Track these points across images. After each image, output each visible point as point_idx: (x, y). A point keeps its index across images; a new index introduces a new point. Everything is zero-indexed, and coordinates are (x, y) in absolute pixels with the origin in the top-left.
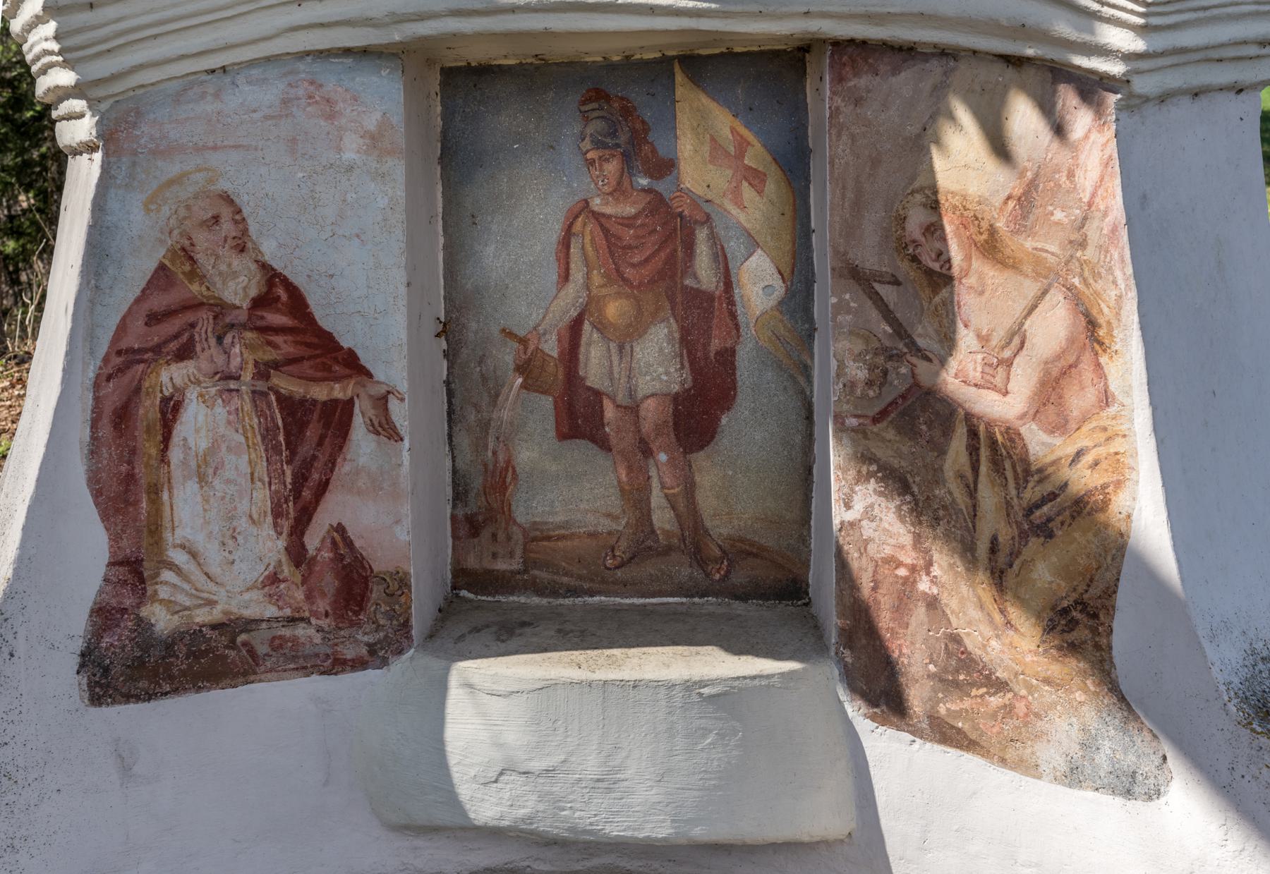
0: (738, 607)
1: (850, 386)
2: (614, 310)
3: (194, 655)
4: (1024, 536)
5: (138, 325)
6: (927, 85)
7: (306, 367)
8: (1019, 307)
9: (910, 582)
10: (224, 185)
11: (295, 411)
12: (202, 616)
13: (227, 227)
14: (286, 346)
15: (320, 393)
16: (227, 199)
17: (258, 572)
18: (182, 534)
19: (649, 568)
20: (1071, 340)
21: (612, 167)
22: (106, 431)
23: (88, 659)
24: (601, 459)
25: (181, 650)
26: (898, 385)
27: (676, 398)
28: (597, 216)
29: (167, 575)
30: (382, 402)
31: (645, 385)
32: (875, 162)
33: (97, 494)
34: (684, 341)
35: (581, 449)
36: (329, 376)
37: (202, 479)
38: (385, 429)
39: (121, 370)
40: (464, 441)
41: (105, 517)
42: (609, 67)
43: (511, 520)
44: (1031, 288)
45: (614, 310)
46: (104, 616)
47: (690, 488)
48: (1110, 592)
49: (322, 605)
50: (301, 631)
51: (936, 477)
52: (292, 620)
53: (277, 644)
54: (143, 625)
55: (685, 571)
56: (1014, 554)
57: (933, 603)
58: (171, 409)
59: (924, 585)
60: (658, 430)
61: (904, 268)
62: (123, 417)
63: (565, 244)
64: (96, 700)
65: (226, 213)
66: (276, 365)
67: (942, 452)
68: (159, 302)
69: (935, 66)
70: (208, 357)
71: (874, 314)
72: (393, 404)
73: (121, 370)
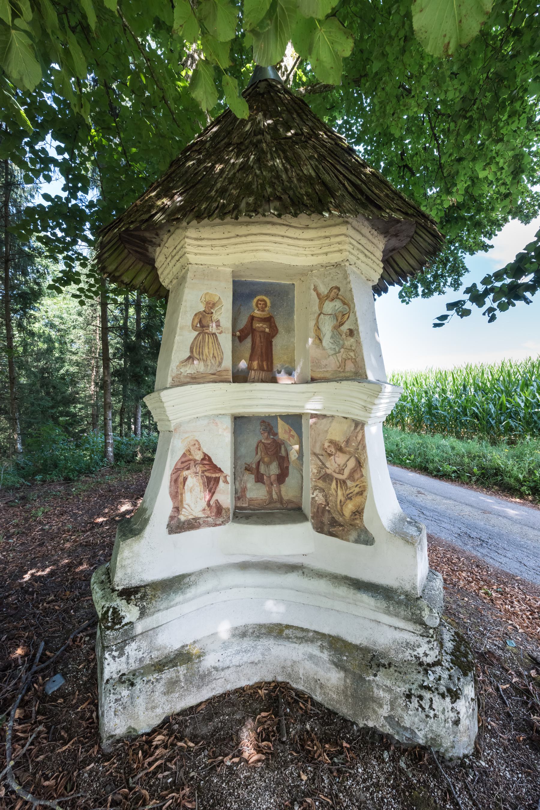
0: (289, 512)
1: (314, 474)
2: (266, 459)
3: (189, 524)
4: (346, 499)
5: (179, 464)
6: (329, 421)
7: (211, 471)
8: (346, 459)
9: (325, 508)
10: (196, 438)
11: (209, 479)
12: (191, 517)
13: (197, 446)
14: (207, 467)
15: (214, 475)
16: (197, 441)
17: (201, 508)
18: (187, 502)
19: (272, 506)
20: (356, 466)
21: (266, 434)
22: (173, 483)
23: (168, 526)
24: (263, 486)
25: (186, 523)
26: (323, 473)
27: (278, 475)
28: (263, 443)
29: (184, 510)
30: (225, 477)
31: (272, 473)
32: (319, 435)
33: (171, 495)
34: (279, 465)
35: (259, 485)
36: (215, 472)
37: (191, 492)
38: (226, 482)
39: (176, 472)
40: (237, 483)
41: (172, 499)
42: (266, 417)
43: (246, 497)
44: (348, 456)
45: (266, 459)
46: (172, 518)
47: (280, 491)
48: (363, 509)
49: (213, 514)
50: (209, 519)
51: (330, 489)
52: (207, 517)
53: (204, 522)
54: (179, 519)
55: (279, 505)
56: (344, 503)
57: (329, 511)
58: (185, 479)
59: (327, 508)
60: (274, 480)
61: (324, 453)
62: (176, 481)
63: (257, 448)
64: (170, 533)
65: (197, 443)
66: (206, 471)
67: (331, 485)
68: (184, 460)
69: (330, 419)
70: (193, 469)
71: (318, 461)
72: (228, 477)
73: (176, 472)
